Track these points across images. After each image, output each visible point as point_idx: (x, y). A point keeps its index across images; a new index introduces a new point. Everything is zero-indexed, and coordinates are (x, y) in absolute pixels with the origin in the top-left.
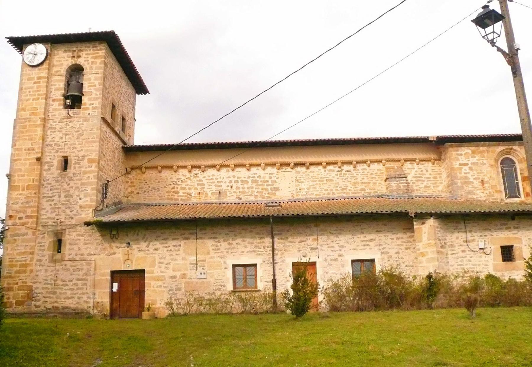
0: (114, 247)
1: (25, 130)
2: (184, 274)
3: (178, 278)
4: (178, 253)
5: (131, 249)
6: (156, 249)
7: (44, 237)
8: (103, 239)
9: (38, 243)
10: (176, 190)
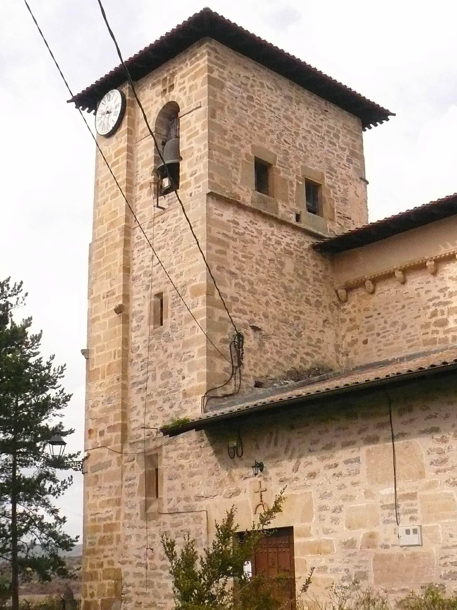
0: (237, 478)
1: (101, 260)
2: (372, 536)
3: (359, 545)
4: (355, 479)
5: (265, 479)
6: (312, 475)
7: (133, 467)
8: (219, 460)
9: (126, 481)
10: (439, 317)
